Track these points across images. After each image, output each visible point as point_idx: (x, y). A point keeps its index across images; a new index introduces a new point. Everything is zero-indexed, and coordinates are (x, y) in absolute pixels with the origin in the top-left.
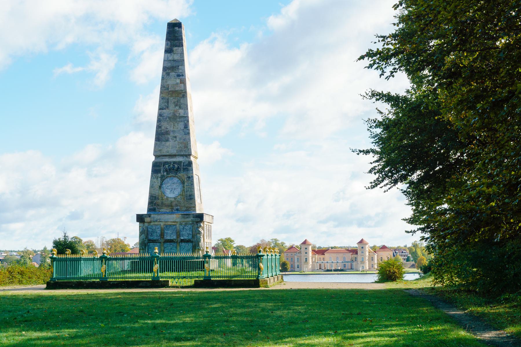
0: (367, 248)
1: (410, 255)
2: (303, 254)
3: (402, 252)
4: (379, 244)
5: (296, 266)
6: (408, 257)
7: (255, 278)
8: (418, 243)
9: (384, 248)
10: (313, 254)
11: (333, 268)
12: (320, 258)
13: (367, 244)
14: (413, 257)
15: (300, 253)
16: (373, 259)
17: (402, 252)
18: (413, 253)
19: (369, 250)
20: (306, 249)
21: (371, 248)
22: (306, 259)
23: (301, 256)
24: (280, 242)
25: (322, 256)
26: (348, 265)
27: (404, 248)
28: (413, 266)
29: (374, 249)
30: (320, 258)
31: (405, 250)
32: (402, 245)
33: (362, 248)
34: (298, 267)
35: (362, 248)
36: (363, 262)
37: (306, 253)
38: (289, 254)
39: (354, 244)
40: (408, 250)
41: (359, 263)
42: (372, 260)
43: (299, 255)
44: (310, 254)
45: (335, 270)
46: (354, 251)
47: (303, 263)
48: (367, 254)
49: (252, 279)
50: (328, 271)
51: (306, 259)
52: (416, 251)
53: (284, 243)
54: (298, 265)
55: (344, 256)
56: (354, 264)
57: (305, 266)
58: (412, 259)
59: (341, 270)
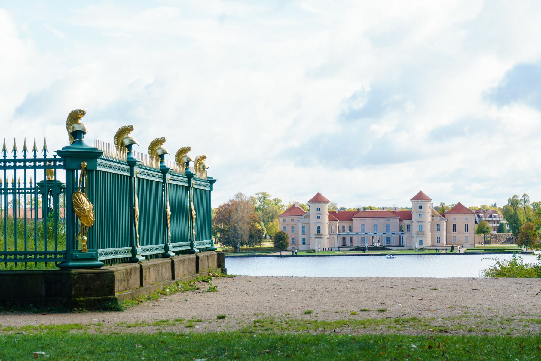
0: (325, 210)
1: (505, 222)
2: (313, 219)
3: (491, 216)
4: (449, 203)
5: (301, 242)
6: (502, 225)
7: (52, 266)
8: (519, 199)
9: (459, 209)
10: (330, 219)
11: (367, 245)
12: (344, 227)
13: (326, 202)
14: (510, 224)
15: (308, 217)
16: (438, 228)
17: (491, 216)
18: (511, 216)
19: (433, 212)
20: (318, 209)
21: (436, 208)
22: (319, 228)
23: (310, 223)
24: (272, 199)
25: (347, 224)
26: (394, 241)
27: (493, 209)
28: (509, 241)
29: (442, 212)
30: (344, 227)
31: (495, 212)
32: (489, 204)
33: (420, 207)
34: (304, 243)
35: (420, 207)
36: (421, 233)
37: (319, 217)
38: (289, 219)
39: (404, 203)
40: (499, 212)
41: (415, 235)
42: (438, 229)
43: (305, 221)
44: (326, 219)
45: (370, 249)
46: (406, 215)
47: (313, 237)
48: (429, 219)
49: (42, 266)
50: (358, 249)
51: (319, 228)
52: (515, 213)
53: (280, 201)
54: (304, 240)
55: (388, 222)
56: (406, 236)
57: (317, 240)
58: (508, 228)
59: (383, 248)
